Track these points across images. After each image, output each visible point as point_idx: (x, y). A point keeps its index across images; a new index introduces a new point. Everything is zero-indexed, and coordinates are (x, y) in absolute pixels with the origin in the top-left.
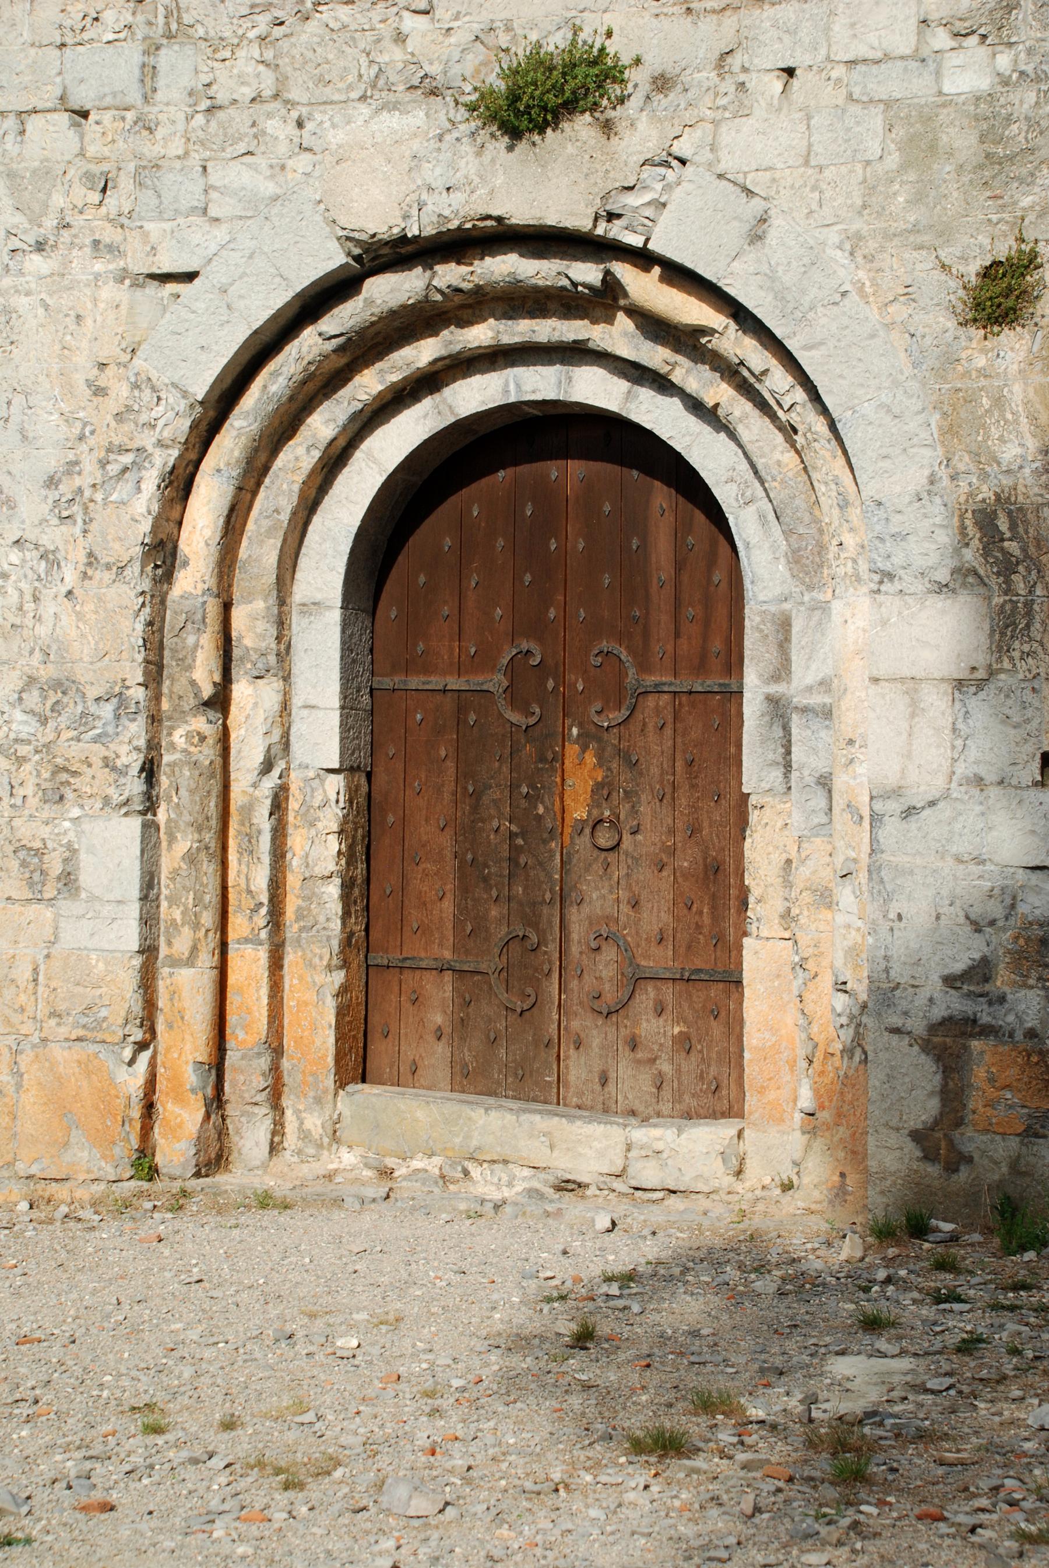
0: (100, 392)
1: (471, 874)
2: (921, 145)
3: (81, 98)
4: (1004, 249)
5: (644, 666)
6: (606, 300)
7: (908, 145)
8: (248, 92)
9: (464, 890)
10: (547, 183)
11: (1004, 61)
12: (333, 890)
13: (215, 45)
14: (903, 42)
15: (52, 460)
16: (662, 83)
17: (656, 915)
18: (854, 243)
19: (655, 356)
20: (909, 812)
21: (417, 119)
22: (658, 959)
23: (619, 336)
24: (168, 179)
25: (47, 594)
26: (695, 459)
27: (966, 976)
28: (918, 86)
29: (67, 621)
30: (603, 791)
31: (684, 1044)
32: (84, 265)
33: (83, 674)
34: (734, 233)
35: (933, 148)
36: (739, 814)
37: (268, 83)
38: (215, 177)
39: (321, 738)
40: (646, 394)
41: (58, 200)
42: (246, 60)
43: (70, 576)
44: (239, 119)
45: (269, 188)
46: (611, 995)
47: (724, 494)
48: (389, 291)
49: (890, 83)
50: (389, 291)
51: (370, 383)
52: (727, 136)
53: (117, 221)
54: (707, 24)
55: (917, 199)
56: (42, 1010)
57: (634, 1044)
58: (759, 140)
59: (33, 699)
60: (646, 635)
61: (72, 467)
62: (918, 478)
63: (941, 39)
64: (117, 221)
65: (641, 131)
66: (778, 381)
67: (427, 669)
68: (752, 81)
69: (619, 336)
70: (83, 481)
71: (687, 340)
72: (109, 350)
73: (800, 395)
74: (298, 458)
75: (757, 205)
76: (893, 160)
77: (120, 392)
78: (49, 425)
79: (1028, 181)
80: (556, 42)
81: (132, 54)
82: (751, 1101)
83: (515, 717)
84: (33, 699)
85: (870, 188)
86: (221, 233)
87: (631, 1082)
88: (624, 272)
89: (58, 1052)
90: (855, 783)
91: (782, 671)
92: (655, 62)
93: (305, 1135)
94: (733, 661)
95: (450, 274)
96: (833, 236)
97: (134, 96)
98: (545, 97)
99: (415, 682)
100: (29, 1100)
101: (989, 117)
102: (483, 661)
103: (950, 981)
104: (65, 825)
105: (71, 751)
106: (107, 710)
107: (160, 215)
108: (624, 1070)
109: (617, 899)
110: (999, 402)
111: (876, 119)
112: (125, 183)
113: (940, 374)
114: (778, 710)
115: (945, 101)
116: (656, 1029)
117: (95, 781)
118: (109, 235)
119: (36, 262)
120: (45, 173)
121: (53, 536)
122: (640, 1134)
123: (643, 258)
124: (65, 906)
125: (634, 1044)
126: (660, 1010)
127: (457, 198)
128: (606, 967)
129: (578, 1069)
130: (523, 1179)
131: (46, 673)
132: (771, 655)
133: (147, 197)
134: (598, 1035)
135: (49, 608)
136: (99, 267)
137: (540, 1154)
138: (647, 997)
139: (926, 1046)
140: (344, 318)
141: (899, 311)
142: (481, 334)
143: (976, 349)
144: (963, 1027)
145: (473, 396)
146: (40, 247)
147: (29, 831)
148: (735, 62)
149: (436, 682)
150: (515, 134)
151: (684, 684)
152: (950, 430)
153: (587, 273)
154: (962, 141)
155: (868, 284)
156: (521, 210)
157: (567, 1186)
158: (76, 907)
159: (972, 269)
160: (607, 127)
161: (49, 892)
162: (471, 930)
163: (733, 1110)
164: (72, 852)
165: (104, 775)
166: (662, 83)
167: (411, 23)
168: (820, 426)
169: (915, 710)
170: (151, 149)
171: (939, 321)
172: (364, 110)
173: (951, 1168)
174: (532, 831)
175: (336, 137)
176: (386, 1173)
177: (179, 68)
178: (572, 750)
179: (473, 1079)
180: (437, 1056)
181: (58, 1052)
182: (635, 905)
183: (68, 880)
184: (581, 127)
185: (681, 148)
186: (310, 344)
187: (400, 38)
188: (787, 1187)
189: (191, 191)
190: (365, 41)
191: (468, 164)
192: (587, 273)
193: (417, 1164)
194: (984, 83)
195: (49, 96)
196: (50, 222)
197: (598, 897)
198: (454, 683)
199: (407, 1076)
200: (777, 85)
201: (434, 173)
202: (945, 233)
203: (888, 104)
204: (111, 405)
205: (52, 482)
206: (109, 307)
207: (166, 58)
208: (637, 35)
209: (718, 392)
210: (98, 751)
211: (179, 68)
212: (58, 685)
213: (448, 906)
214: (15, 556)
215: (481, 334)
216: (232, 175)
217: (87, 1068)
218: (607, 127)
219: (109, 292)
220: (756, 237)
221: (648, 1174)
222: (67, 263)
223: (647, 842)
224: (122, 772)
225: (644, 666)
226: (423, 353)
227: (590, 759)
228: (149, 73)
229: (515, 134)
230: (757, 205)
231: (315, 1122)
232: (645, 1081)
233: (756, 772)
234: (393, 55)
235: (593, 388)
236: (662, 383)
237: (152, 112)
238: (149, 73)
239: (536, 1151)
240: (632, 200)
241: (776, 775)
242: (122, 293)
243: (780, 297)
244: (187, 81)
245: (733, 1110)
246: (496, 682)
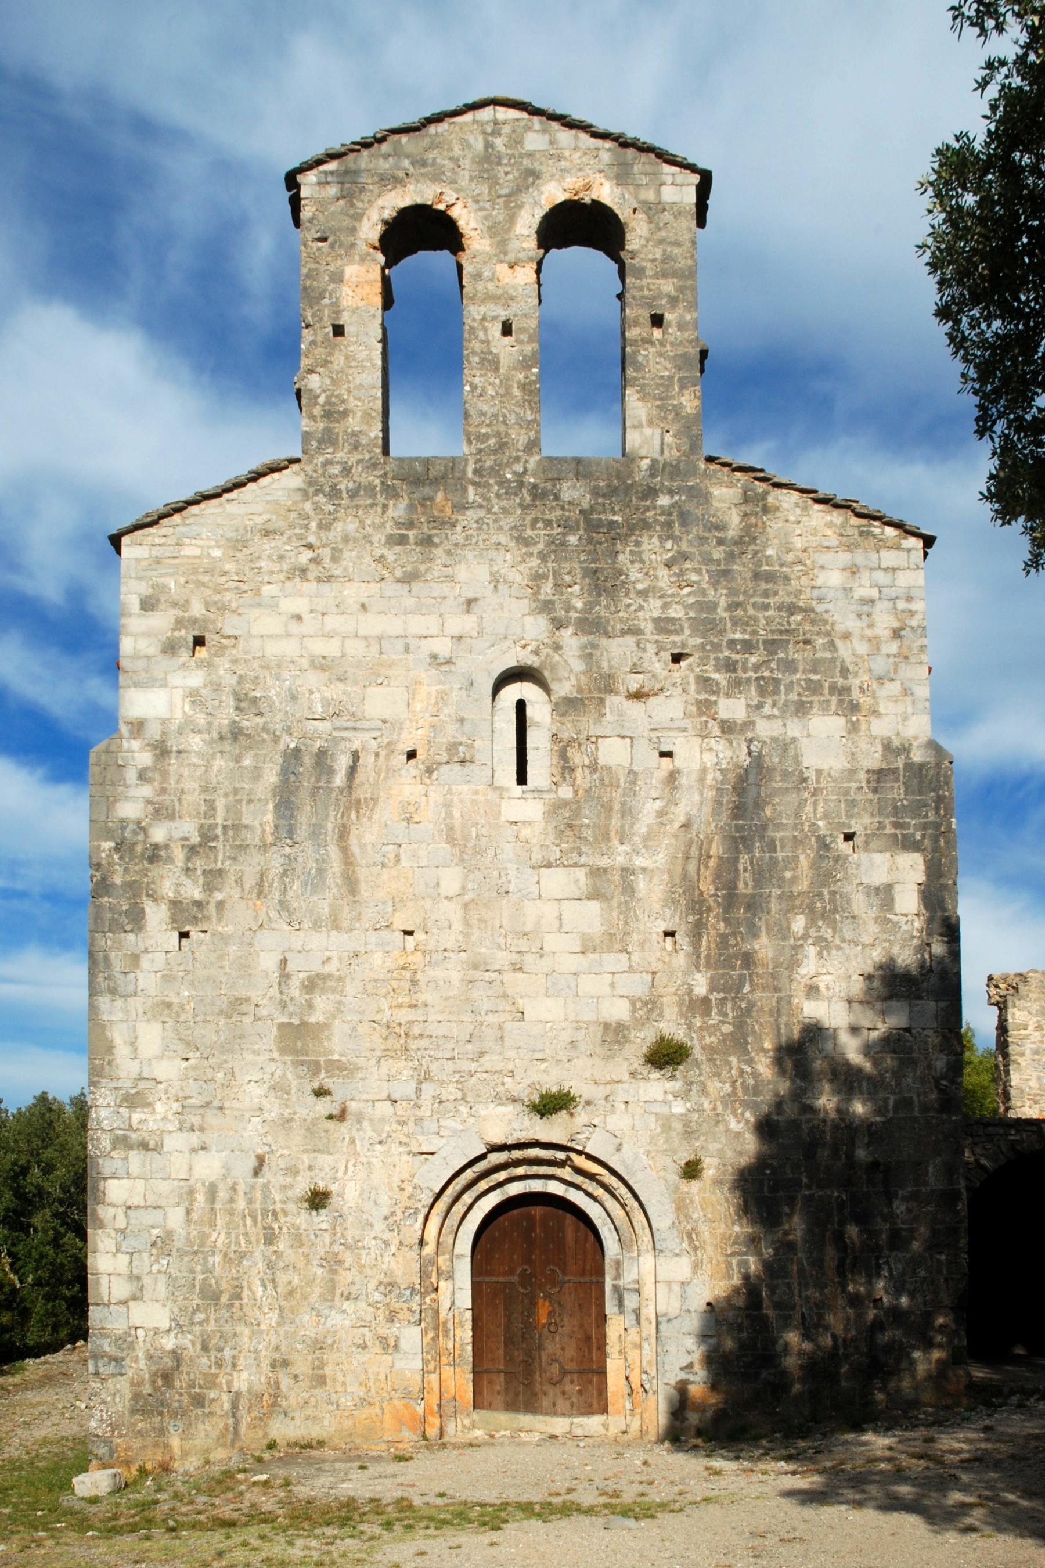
0: (402, 1189)
1: (509, 1342)
2: (666, 1128)
3: (394, 1097)
4: (692, 1157)
5: (564, 1273)
6: (561, 1164)
7: (663, 1126)
8: (452, 1097)
9: (506, 1347)
10: (553, 1130)
11: (688, 1105)
12: (470, 1348)
13: (442, 1083)
14: (660, 1097)
15: (386, 1212)
16: (588, 1103)
17: (571, 1352)
18: (648, 1153)
19: (579, 1179)
20: (669, 1320)
21: (510, 1109)
22: (572, 1366)
23: (566, 1173)
24: (426, 1123)
25: (386, 1255)
26: (588, 1211)
27: (686, 1367)
29: (393, 1264)
30: (551, 1314)
31: (580, 1392)
32: (396, 1149)
33: (399, 1281)
34: (612, 1149)
35: (670, 1127)
36: (602, 1318)
38: (442, 1123)
39: (465, 1299)
40: (572, 1190)
41: (387, 1128)
42: (452, 1088)
43: (393, 1249)
44: (450, 1106)
45: (461, 1127)
46: (556, 1379)
47: (598, 1222)
48: (496, 1158)
49: (657, 1108)
50: (496, 1158)
51: (483, 1185)
52: (609, 1120)
54: (601, 1087)
55: (666, 1142)
56: (389, 1389)
57: (563, 1393)
58: (618, 1121)
59: (382, 1288)
60: (565, 1264)
61: (393, 1214)
62: (669, 1223)
63: (670, 1097)
64: (408, 1136)
65: (582, 1116)
66: (622, 1191)
67: (491, 1275)
68: (616, 1104)
69: (566, 1173)
70: (397, 1218)
71: (591, 1177)
72: (405, 1176)
73: (630, 1195)
74: (459, 1208)
75: (618, 1141)
76: (659, 1130)
77: (409, 1189)
78: (384, 1199)
79: (697, 1139)
80: (554, 1089)
81: (413, 1084)
82: (610, 1408)
83: (522, 1290)
84: (382, 1288)
85: (652, 1138)
86: (444, 1141)
87: (562, 1404)
88: (573, 1155)
89: (396, 1402)
90: (649, 1312)
91: (618, 1276)
92: (586, 1096)
93: (464, 1426)
94: (600, 1272)
95: (517, 1154)
96: (642, 1150)
97: (414, 1097)
98: (551, 1105)
99: (487, 1279)
100: (387, 1417)
102: (511, 1272)
103: (682, 1369)
104: (394, 1329)
106: (408, 1292)
107: (423, 1134)
108: (560, 1401)
109: (558, 1347)
110: (692, 1201)
111: (653, 1118)
112: (411, 1124)
113: (675, 1192)
114: (618, 1291)
115: (673, 1115)
116: (572, 1388)
117: (404, 1315)
118: (405, 1140)
119: (378, 1147)
120: (382, 1120)
121: (387, 1236)
122: (576, 1420)
123: (580, 1153)
124: (396, 1355)
125: (563, 1393)
126: (572, 1382)
127: (524, 1133)
128: (555, 1369)
129: (546, 1402)
130: (537, 1437)
131: (386, 1280)
132: (613, 1272)
133: (418, 1128)
134: (551, 1390)
135: (386, 1259)
136: (401, 1149)
137: (544, 1428)
138: (567, 1379)
140: (481, 1166)
142: (520, 1171)
143: (685, 1186)
145: (515, 1189)
146: (380, 1143)
147: (382, 1332)
148: (611, 1099)
149: (494, 1279)
150: (542, 1115)
151: (577, 1280)
152: (678, 1209)
153: (561, 1155)
154: (678, 1126)
156: (544, 1138)
157: (553, 1437)
158: (400, 1356)
159: (683, 1163)
160: (572, 1115)
162: (510, 1360)
163: (604, 1410)
166: (588, 1103)
167: (506, 1079)
168: (636, 1204)
169: (670, 1290)
170: (420, 1113)
171: (674, 1178)
172: (492, 1105)
174: (529, 1327)
176: (492, 1437)
178: (541, 1301)
179: (512, 1406)
180: (499, 1400)
181: (396, 1402)
182: (563, 1349)
183: (396, 1347)
184: (564, 1113)
186: (469, 1174)
187: (503, 1084)
188: (624, 1432)
189: (434, 1127)
190: (492, 1084)
191: (527, 1123)
192: (561, 1155)
193: (503, 1433)
194: (683, 1111)
195: (384, 1095)
196: (384, 1135)
197: (551, 1347)
198: (501, 1279)
199: (490, 1407)
200: (623, 1106)
201: (516, 1125)
202: (675, 1152)
203: (656, 1114)
204: (406, 1194)
205: (386, 1218)
206: (405, 1164)
207: (424, 1086)
208: (579, 1088)
209: (599, 1192)
210: (406, 1305)
212: (390, 1284)
213: (501, 1352)
214: (373, 1242)
215: (520, 1171)
216: (447, 1122)
217: (406, 1406)
218: (572, 1115)
219: (405, 1157)
220: (618, 1150)
221: (579, 1432)
222: (390, 1148)
223: (566, 1330)
224: (414, 1312)
225: (564, 1273)
226: (502, 1176)
227: (547, 1304)
228: (418, 1091)
229: (542, 1115)
231: (467, 1422)
232: (568, 1405)
233: (610, 1307)
234: (500, 1089)
235: (554, 1188)
236: (577, 1187)
237: (420, 1102)
238: (418, 1091)
239: (541, 1427)
240: (579, 1136)
241: (616, 1309)
242: (410, 1158)
243: (626, 1167)
244: (432, 1093)
245: (604, 1410)
246: (515, 1279)
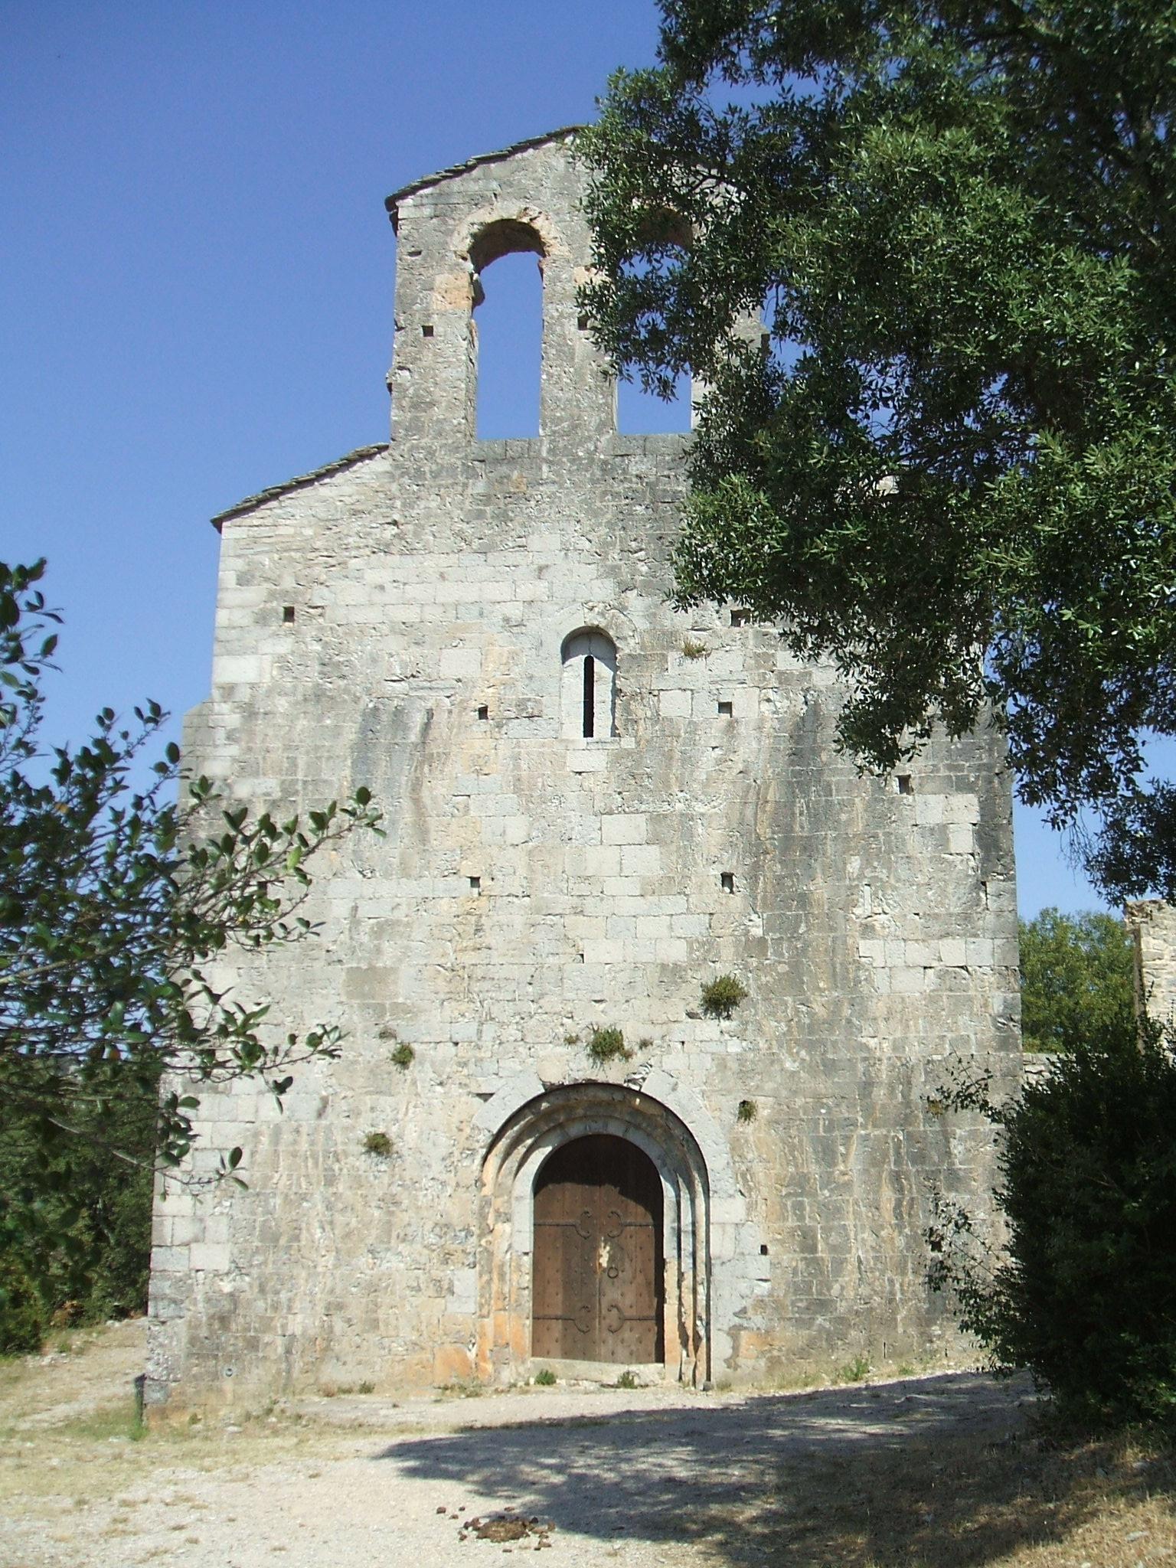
2: (722, 1064)
10: (613, 1072)
11: (744, 1044)
15: (444, 1152)
17: (630, 1299)
24: (485, 1064)
28: (720, 1049)
32: (455, 1090)
33: (455, 1221)
34: (667, 1088)
37: (519, 1036)
41: (448, 1070)
43: (450, 1190)
44: (510, 1047)
45: (520, 1068)
49: (713, 1047)
53: (468, 1076)
54: (658, 1027)
58: (675, 1061)
59: (437, 1229)
63: (727, 1037)
72: (464, 1117)
75: (674, 1080)
77: (468, 1131)
81: (475, 1025)
84: (437, 1229)
86: (503, 1081)
89: (448, 1346)
96: (697, 1090)
97: (475, 1038)
100: (438, 1362)
101: (740, 1059)
105: (452, 1247)
109: (623, 1295)
118: (466, 1081)
119: (439, 1088)
121: (444, 1177)
125: (622, 1341)
131: (443, 1221)
134: (610, 1339)
139: (728, 1334)
141: (717, 1113)
144: (739, 1328)
146: (441, 1084)
152: (733, 1149)
154: (734, 1066)
155: (140, 853)
161: (444, 1293)
164: (451, 1282)
165: (462, 1255)
173: (736, 1369)
175: (541, 1053)
177: (490, 1031)
181: (448, 1346)
185: (651, 1062)
194: (739, 1050)
205: (443, 1159)
210: (461, 1247)
211: (490, 1031)
213: (560, 1296)
217: (457, 1351)
220: (674, 1089)
228: (480, 1032)
230: (674, 1080)
232: (627, 1353)
238: (480, 1032)
